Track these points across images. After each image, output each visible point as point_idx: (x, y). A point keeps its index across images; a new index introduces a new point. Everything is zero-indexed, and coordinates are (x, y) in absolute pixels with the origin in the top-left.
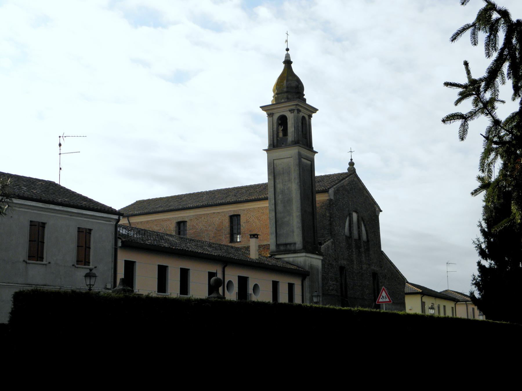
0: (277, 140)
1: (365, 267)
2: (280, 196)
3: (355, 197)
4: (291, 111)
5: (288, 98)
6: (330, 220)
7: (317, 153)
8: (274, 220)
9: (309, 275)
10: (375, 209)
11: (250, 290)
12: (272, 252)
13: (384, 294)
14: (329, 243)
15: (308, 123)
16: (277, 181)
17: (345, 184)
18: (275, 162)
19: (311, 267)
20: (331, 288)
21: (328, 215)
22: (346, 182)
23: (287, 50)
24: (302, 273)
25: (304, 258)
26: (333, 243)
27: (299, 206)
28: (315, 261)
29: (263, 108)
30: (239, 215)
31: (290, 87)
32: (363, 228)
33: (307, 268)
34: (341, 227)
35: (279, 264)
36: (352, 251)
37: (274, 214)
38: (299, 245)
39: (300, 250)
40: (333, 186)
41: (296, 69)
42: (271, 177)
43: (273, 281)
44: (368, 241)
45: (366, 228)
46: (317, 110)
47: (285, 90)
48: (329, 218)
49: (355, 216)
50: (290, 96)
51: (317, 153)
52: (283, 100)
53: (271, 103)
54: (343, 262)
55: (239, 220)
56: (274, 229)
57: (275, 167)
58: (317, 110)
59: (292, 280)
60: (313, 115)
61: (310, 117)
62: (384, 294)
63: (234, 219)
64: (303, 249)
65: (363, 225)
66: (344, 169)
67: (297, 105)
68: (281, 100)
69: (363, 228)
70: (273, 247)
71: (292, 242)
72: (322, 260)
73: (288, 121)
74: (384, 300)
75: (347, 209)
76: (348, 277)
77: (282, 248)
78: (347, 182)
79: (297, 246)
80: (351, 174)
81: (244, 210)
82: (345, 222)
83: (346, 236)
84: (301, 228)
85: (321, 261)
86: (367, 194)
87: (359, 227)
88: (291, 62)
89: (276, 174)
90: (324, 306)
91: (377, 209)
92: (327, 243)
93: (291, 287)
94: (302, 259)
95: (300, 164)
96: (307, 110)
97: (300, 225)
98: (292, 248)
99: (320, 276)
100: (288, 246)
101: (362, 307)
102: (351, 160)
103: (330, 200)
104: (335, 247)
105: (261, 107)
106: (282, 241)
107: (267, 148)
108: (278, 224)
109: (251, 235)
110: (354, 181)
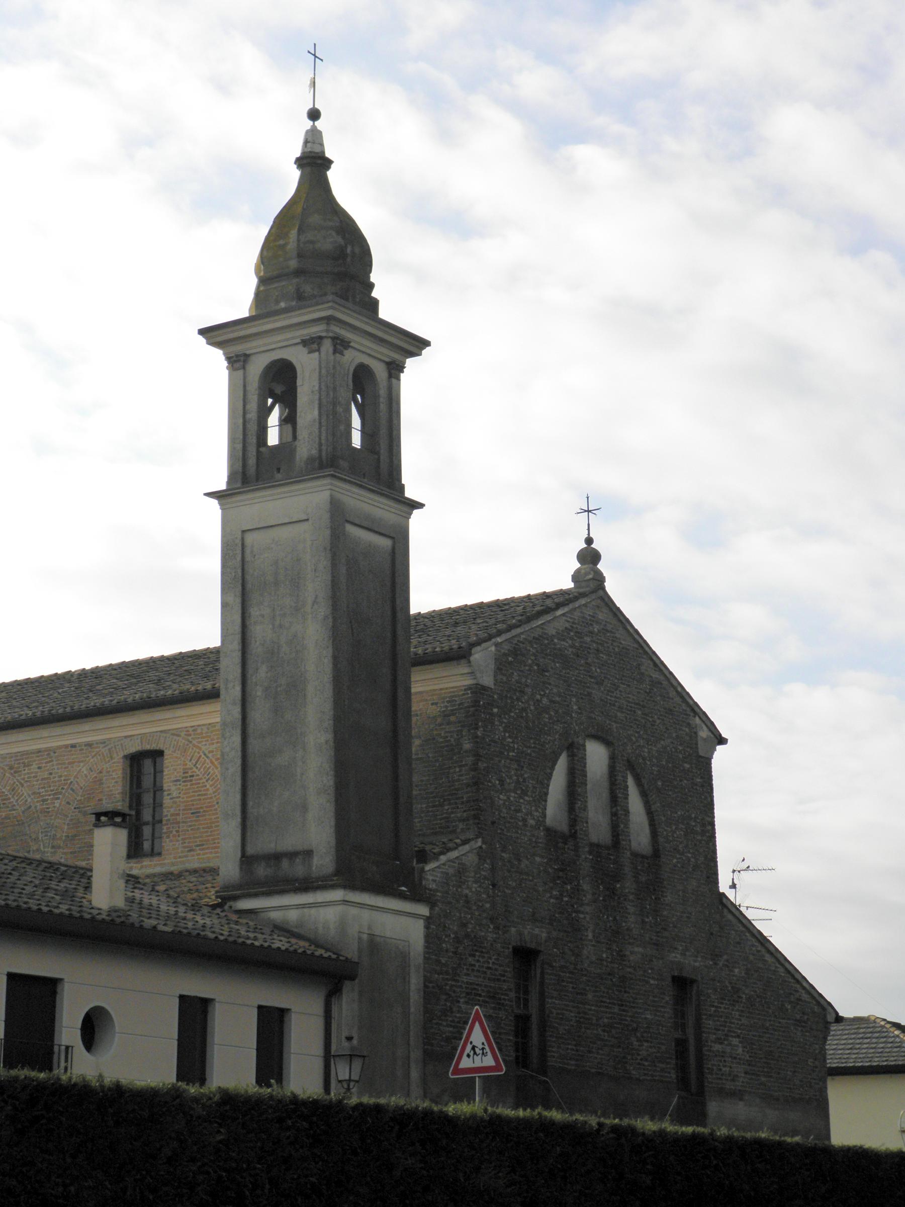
0: (259, 453)
1: (636, 953)
2: (263, 669)
3: (600, 683)
4: (312, 343)
5: (300, 296)
6: (475, 768)
7: (420, 506)
8: (239, 762)
9: (352, 978)
11: (68, 1031)
12: (226, 888)
13: (477, 1037)
14: (465, 853)
15: (383, 392)
16: (254, 612)
17: (551, 631)
18: (250, 538)
19: (374, 945)
21: (467, 746)
22: (556, 623)
23: (314, 115)
24: (327, 971)
25: (340, 908)
27: (328, 707)
28: (400, 924)
29: (213, 334)
30: (160, 753)
31: (317, 256)
32: (635, 804)
33: (351, 952)
35: (243, 931)
37: (237, 739)
38: (324, 861)
39: (325, 878)
40: (490, 638)
41: (343, 187)
42: (230, 599)
43: (260, 1007)
46: (425, 343)
47: (293, 264)
48: (470, 760)
49: (596, 756)
50: (308, 289)
51: (420, 506)
52: (283, 305)
53: (247, 315)
54: (534, 934)
55: (158, 772)
56: (238, 797)
57: (248, 557)
58: (425, 343)
59: (275, 995)
60: (410, 362)
61: (395, 369)
62: (477, 1037)
63: (142, 764)
64: (338, 872)
66: (557, 575)
67: (329, 319)
68: (277, 302)
69: (635, 804)
70: (230, 869)
71: (299, 848)
72: (428, 921)
73: (299, 382)
74: (478, 1062)
75: (558, 727)
77: (262, 871)
78: (561, 625)
79: (316, 861)
80: (583, 595)
81: (176, 733)
82: (549, 777)
83: (548, 830)
84: (332, 791)
85: (421, 924)
86: (656, 675)
87: (616, 798)
88: (328, 163)
89: (249, 586)
91: (704, 733)
92: (454, 854)
94: (332, 914)
95: (337, 544)
96: (382, 341)
97: (329, 781)
98: (298, 869)
99: (415, 982)
100: (285, 863)
101: (371, 1096)
102: (589, 541)
103: (478, 690)
104: (493, 869)
105: (202, 332)
106: (265, 842)
107: (223, 487)
108: (249, 775)
109: (98, 815)
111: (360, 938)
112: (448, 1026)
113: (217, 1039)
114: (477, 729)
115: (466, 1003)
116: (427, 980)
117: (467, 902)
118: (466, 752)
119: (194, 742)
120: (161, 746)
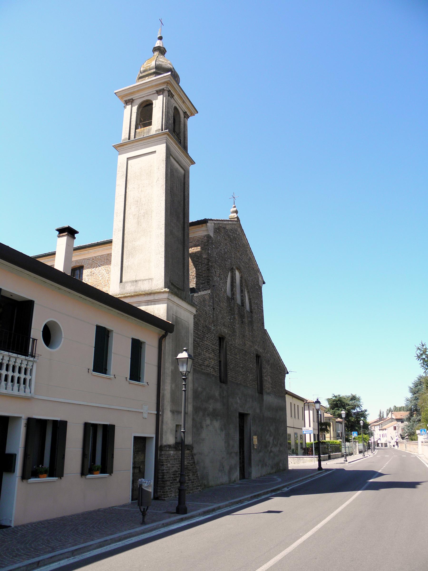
1: (248, 343)
10: (258, 282)
20: (206, 363)
21: (204, 256)
26: (212, 297)
34: (221, 279)
36: (234, 318)
44: (251, 312)
45: (249, 296)
65: (246, 292)
76: (228, 353)
79: (154, 282)
83: (228, 297)
90: (335, 441)
93: (137, 347)
110: (236, 231)
111: (173, 317)
112: (200, 360)
113: (113, 351)
114: (208, 250)
115: (206, 352)
116: (194, 340)
117: (206, 313)
118: (204, 258)
119: (95, 262)
120: (83, 264)
